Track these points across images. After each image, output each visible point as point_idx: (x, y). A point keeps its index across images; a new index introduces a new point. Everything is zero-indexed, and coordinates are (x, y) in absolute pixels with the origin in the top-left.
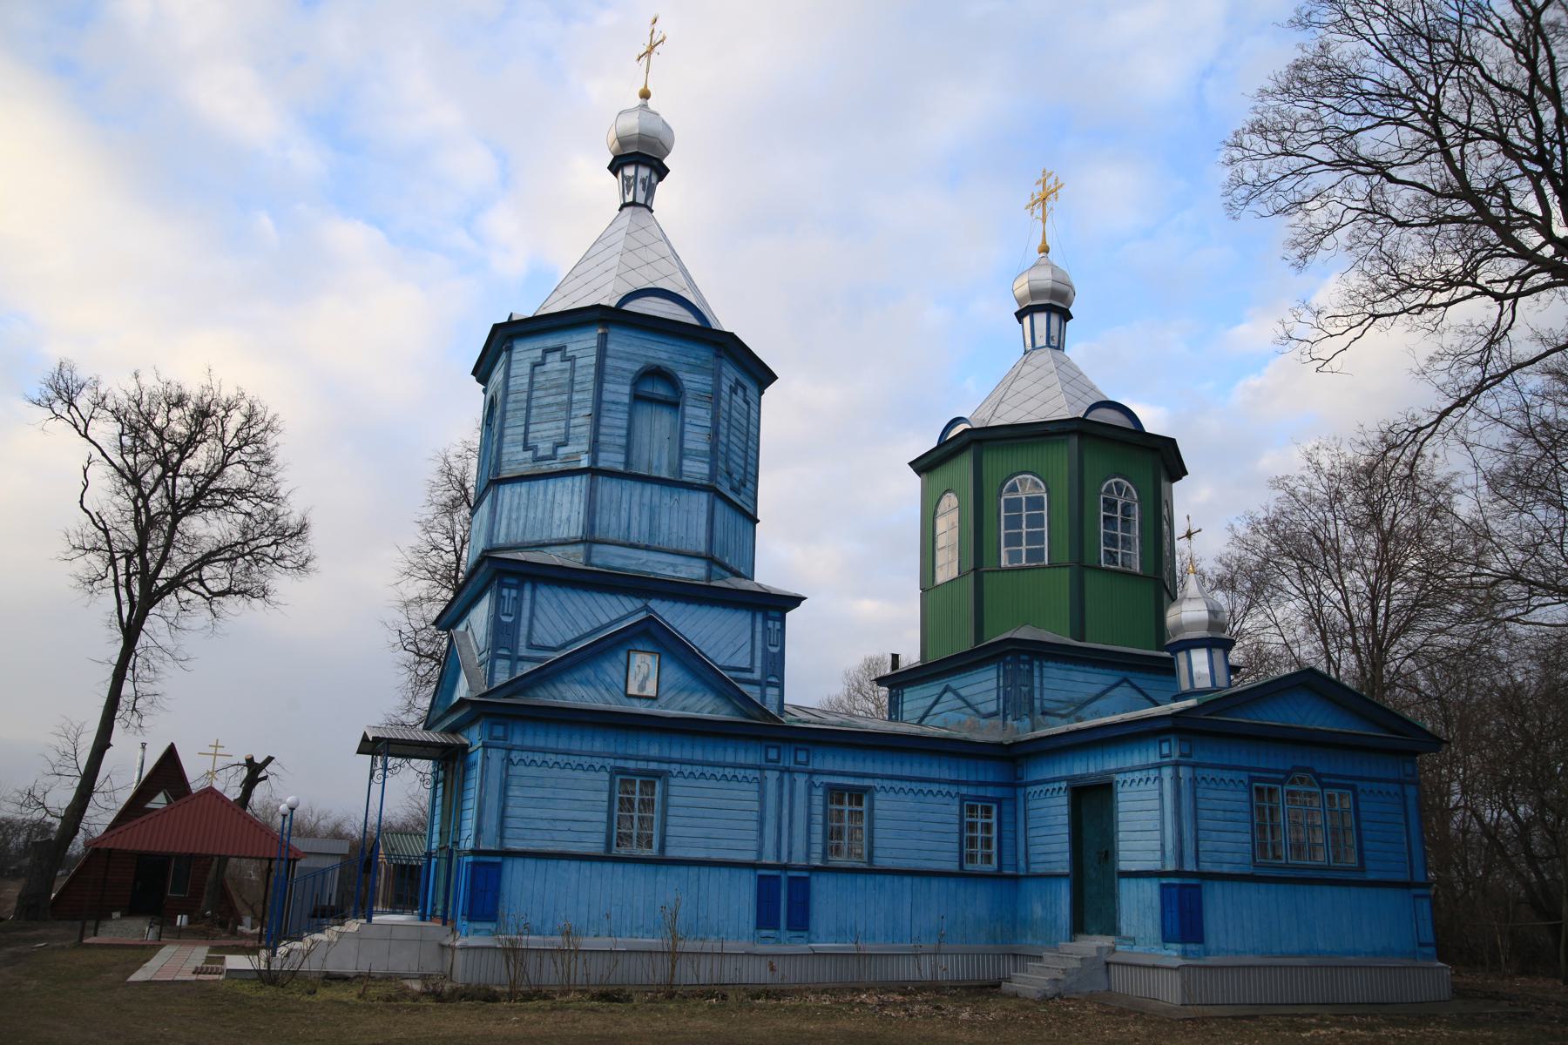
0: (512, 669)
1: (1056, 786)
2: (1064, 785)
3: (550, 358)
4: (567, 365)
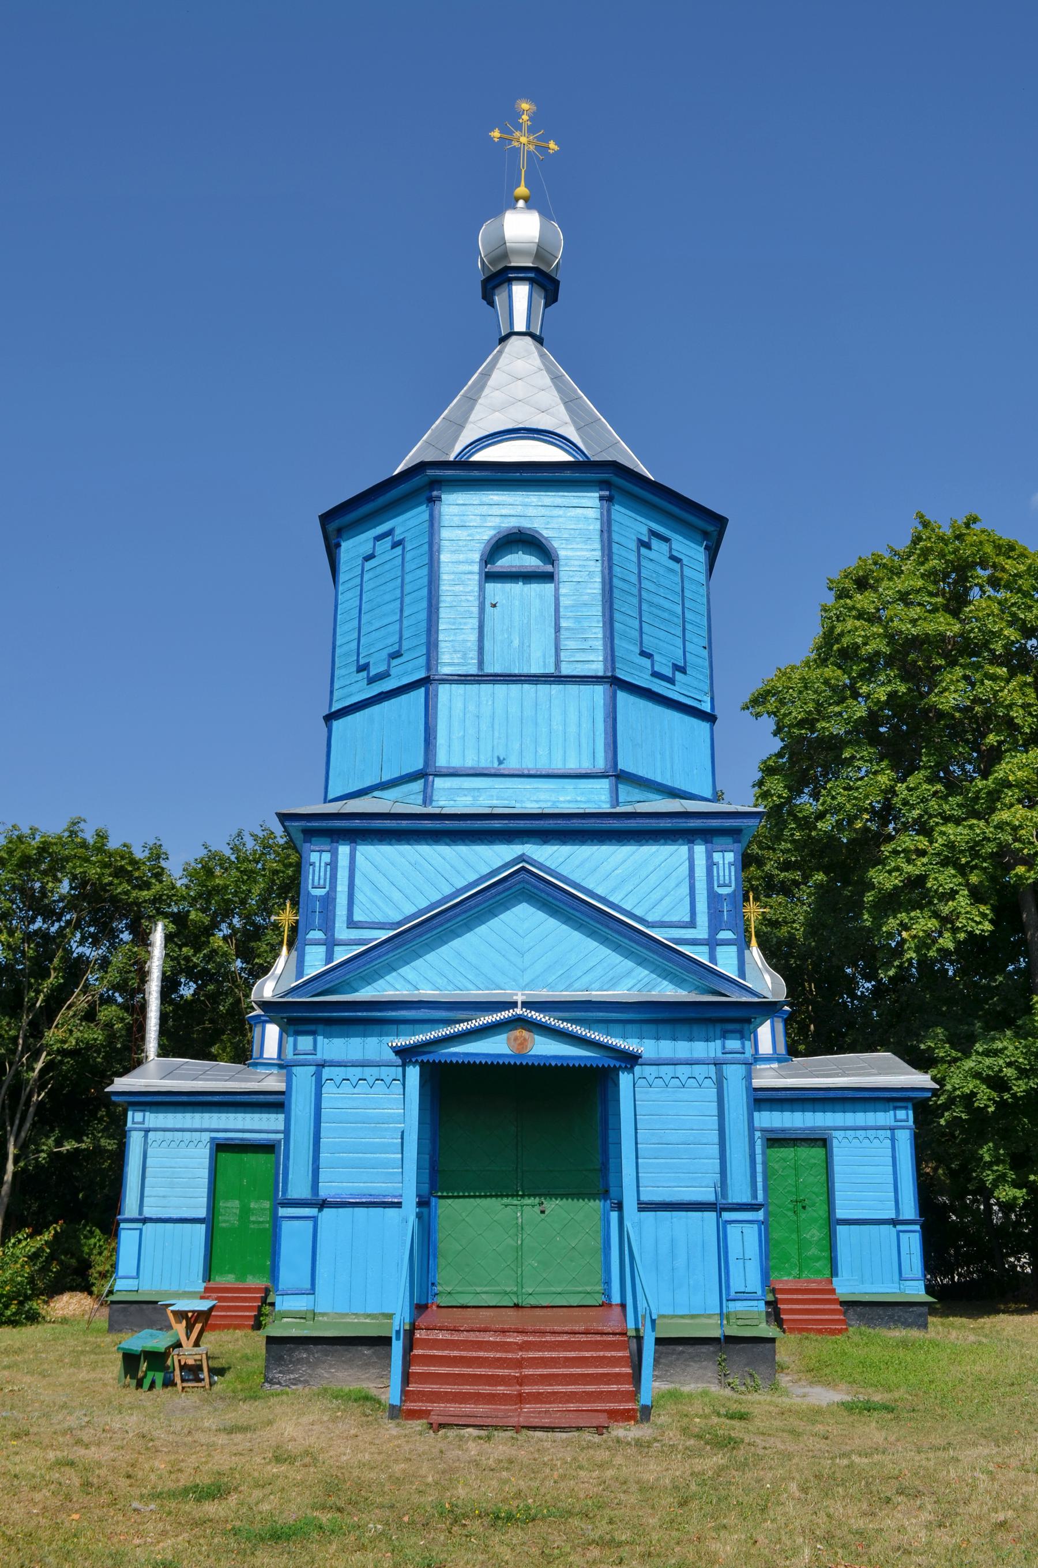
0: (329, 958)
3: (655, 543)
4: (676, 566)
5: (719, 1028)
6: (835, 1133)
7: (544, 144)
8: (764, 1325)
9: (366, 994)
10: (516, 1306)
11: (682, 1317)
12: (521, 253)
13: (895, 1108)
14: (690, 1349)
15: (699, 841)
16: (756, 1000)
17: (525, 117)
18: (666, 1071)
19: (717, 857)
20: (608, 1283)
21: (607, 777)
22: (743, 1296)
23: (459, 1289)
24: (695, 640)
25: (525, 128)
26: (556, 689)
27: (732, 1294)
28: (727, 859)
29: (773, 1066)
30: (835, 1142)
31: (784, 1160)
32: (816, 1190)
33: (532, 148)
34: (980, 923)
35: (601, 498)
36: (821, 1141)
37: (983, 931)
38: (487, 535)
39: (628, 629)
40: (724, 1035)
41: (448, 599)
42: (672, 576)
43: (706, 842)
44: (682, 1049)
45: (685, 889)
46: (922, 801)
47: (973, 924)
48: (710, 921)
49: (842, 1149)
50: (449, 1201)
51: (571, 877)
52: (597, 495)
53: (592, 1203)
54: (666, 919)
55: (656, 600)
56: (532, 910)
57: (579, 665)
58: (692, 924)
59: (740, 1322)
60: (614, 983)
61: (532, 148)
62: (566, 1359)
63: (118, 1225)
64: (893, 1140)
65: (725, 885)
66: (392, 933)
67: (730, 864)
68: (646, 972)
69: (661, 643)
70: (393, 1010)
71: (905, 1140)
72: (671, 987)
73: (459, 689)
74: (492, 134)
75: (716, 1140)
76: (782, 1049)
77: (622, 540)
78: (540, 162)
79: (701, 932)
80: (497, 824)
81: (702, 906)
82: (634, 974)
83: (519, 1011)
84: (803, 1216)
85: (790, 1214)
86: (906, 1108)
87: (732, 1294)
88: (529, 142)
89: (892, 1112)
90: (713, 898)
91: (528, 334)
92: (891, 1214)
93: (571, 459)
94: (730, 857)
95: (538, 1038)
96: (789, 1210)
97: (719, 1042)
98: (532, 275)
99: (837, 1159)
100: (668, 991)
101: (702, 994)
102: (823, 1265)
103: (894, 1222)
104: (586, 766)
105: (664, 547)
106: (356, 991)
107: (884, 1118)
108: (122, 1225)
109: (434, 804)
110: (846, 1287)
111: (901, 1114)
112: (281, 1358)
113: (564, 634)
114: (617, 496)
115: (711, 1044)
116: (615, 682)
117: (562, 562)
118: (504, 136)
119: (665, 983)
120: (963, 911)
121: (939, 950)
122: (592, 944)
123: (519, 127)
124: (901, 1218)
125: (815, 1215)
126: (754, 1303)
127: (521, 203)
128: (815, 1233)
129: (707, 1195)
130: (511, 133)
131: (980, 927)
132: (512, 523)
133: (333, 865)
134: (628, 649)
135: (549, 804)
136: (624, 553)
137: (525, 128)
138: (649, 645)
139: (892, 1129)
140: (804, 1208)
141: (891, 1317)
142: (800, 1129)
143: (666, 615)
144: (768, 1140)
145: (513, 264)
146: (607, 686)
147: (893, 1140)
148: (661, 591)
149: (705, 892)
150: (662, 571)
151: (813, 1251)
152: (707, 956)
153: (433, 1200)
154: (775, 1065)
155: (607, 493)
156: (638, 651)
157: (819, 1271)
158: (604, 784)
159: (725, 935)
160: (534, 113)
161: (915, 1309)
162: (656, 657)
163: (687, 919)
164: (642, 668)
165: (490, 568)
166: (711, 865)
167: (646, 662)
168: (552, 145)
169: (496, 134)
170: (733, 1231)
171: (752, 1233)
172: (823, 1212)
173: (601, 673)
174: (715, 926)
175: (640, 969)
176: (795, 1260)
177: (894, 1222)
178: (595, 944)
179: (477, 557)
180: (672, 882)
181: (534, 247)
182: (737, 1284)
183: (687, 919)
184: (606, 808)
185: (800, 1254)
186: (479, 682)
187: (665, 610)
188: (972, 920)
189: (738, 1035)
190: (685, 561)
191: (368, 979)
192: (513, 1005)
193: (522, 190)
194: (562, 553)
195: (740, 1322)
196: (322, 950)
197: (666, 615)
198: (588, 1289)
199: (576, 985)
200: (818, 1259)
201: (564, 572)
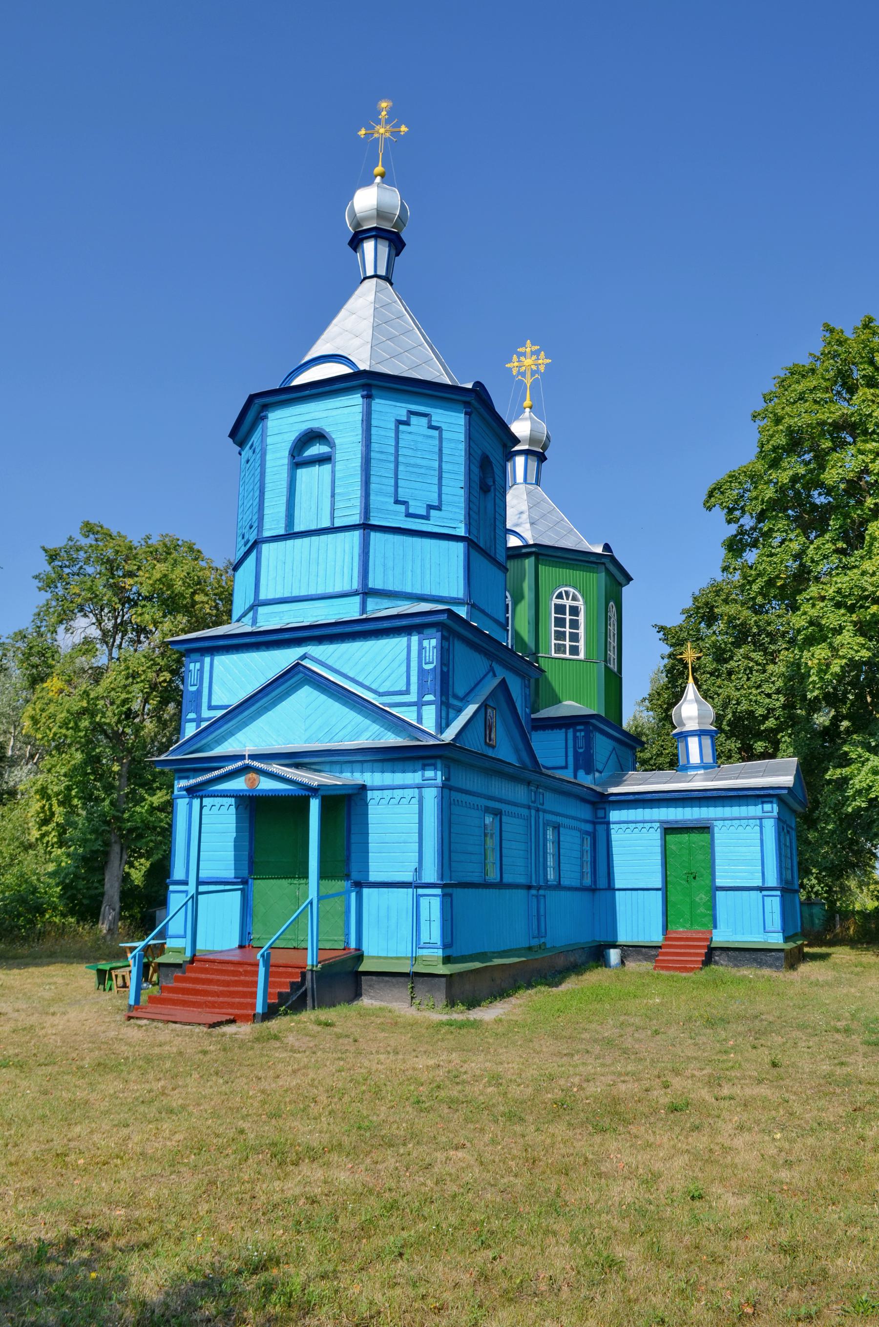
0: (198, 726)
1: (653, 825)
2: (658, 825)
3: (414, 420)
4: (436, 433)
5: (421, 762)
6: (715, 823)
7: (397, 130)
8: (441, 966)
9: (218, 751)
10: (295, 948)
11: (391, 958)
12: (367, 219)
13: (763, 803)
14: (394, 980)
15: (415, 633)
16: (439, 742)
17: (384, 113)
18: (387, 793)
19: (425, 643)
20: (347, 935)
21: (358, 594)
22: (429, 945)
23: (264, 936)
24: (452, 483)
25: (383, 122)
26: (330, 537)
27: (422, 945)
28: (432, 644)
29: (699, 772)
30: (716, 830)
31: (680, 843)
32: (703, 865)
33: (388, 135)
34: (857, 651)
35: (363, 397)
36: (705, 829)
37: (861, 657)
38: (292, 436)
39: (383, 487)
40: (423, 769)
41: (270, 485)
42: (430, 441)
43: (419, 633)
44: (399, 778)
45: (404, 668)
46: (825, 558)
47: (853, 653)
48: (418, 689)
49: (721, 834)
50: (259, 881)
51: (334, 666)
52: (359, 395)
53: (339, 883)
54: (391, 690)
55: (412, 461)
56: (311, 690)
57: (345, 519)
58: (407, 692)
59: (425, 963)
60: (358, 736)
61: (388, 135)
62: (218, 981)
63: (167, 888)
64: (761, 827)
65: (429, 663)
66: (225, 711)
67: (434, 647)
68: (378, 727)
69: (417, 492)
70: (215, 762)
71: (770, 826)
72: (393, 736)
73: (273, 545)
74: (360, 133)
75: (417, 840)
76: (709, 759)
77: (382, 424)
78: (395, 143)
79: (413, 697)
80: (286, 636)
81: (414, 679)
82: (371, 728)
83: (247, 762)
84: (694, 884)
85: (684, 882)
86: (771, 802)
87: (422, 945)
88: (386, 131)
89: (760, 806)
90: (421, 671)
91: (376, 276)
92: (758, 883)
93: (351, 371)
94: (434, 642)
95: (262, 779)
96: (684, 879)
97: (420, 773)
98: (374, 233)
99: (717, 842)
100: (392, 739)
101: (412, 740)
102: (707, 920)
103: (761, 889)
104: (347, 588)
105: (424, 421)
106: (212, 749)
107: (754, 810)
108: (172, 888)
109: (258, 625)
110: (720, 937)
111: (768, 807)
112: (168, 976)
113: (337, 498)
114: (374, 392)
115: (416, 774)
116: (366, 527)
117: (337, 447)
118: (369, 132)
119: (390, 733)
120: (846, 643)
121: (832, 674)
122: (345, 710)
123: (378, 122)
124: (766, 886)
125: (703, 883)
126: (436, 950)
127: (378, 179)
128: (702, 897)
129: (408, 877)
130: (373, 128)
131: (859, 654)
132: (305, 427)
133: (201, 670)
134: (381, 501)
135: (323, 617)
136: (382, 433)
137: (383, 122)
138: (403, 495)
139: (761, 819)
140: (695, 878)
141: (755, 960)
142: (689, 820)
143: (422, 471)
144: (665, 829)
145: (365, 228)
146: (362, 531)
147: (761, 827)
148: (419, 454)
149: (416, 669)
150: (420, 439)
151: (702, 910)
152: (415, 715)
153: (250, 881)
154: (702, 772)
155: (365, 393)
156: (392, 500)
157: (704, 925)
158: (357, 600)
159: (430, 697)
160: (391, 108)
161: (773, 953)
162: (411, 503)
163: (404, 689)
164: (396, 513)
165: (297, 459)
166: (421, 648)
167: (402, 508)
168: (404, 129)
169: (362, 132)
170: (424, 902)
171: (436, 903)
172: (708, 882)
173: (358, 523)
174: (421, 694)
175: (374, 725)
176: (688, 916)
177: (761, 889)
178: (347, 710)
179: (286, 453)
180: (395, 665)
181: (375, 212)
182: (425, 938)
183: (404, 689)
184: (356, 616)
185: (691, 912)
186: (286, 539)
187: (421, 467)
188: (852, 648)
189: (433, 767)
190: (444, 427)
191: (219, 741)
192: (242, 757)
193: (379, 169)
194: (337, 441)
195: (425, 963)
196: (194, 724)
197: (422, 471)
198: (336, 938)
199: (335, 738)
200: (705, 916)
201: (338, 456)
